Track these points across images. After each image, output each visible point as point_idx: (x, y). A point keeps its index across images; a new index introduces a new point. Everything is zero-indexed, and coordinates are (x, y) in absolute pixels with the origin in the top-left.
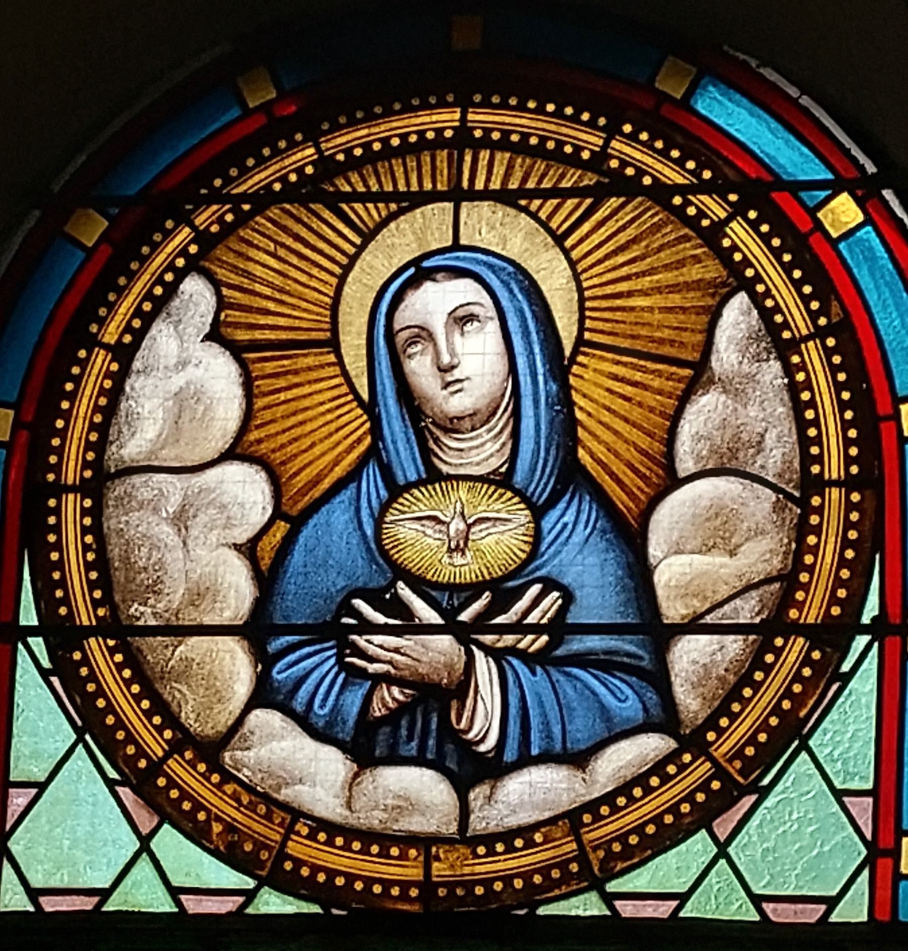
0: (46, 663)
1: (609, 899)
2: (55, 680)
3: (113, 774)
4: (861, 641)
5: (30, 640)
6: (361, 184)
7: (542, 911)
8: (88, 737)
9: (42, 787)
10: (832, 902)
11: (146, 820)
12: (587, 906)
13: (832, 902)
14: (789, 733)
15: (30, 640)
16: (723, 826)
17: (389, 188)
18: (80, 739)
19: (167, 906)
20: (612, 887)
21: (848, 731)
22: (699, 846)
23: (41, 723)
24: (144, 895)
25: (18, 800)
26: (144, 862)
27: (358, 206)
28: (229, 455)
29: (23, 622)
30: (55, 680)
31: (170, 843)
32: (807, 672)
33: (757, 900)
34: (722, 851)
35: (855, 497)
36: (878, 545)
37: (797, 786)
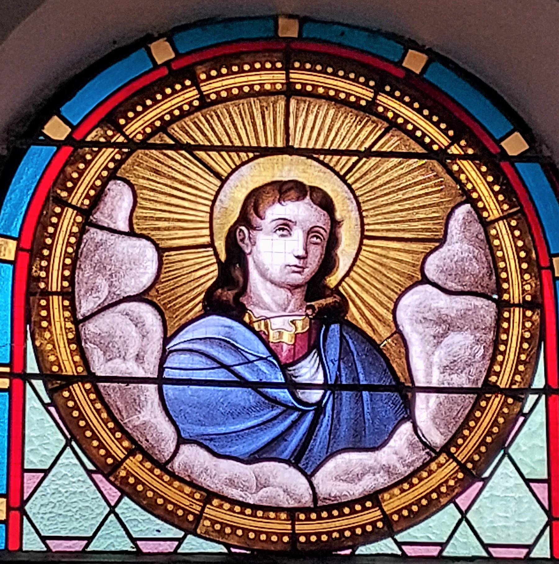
0: (47, 400)
1: (400, 545)
2: (52, 409)
3: (90, 467)
4: (532, 398)
5: (34, 382)
6: (238, 140)
7: (362, 550)
8: (73, 443)
9: (46, 472)
10: (530, 547)
11: (113, 494)
12: (386, 546)
13: (530, 547)
14: (498, 443)
15: (34, 382)
16: (463, 501)
17: (254, 144)
18: (68, 444)
19: (128, 546)
20: (399, 537)
21: (530, 445)
22: (448, 516)
23: (43, 435)
24: (113, 540)
25: (30, 481)
26: (112, 517)
27: (233, 154)
28: (140, 298)
29: (29, 371)
30: (52, 409)
31: (127, 509)
32: (405, 513)
33: (486, 546)
34: (464, 514)
35: (286, 539)
36: (543, 338)
37: (503, 478)
